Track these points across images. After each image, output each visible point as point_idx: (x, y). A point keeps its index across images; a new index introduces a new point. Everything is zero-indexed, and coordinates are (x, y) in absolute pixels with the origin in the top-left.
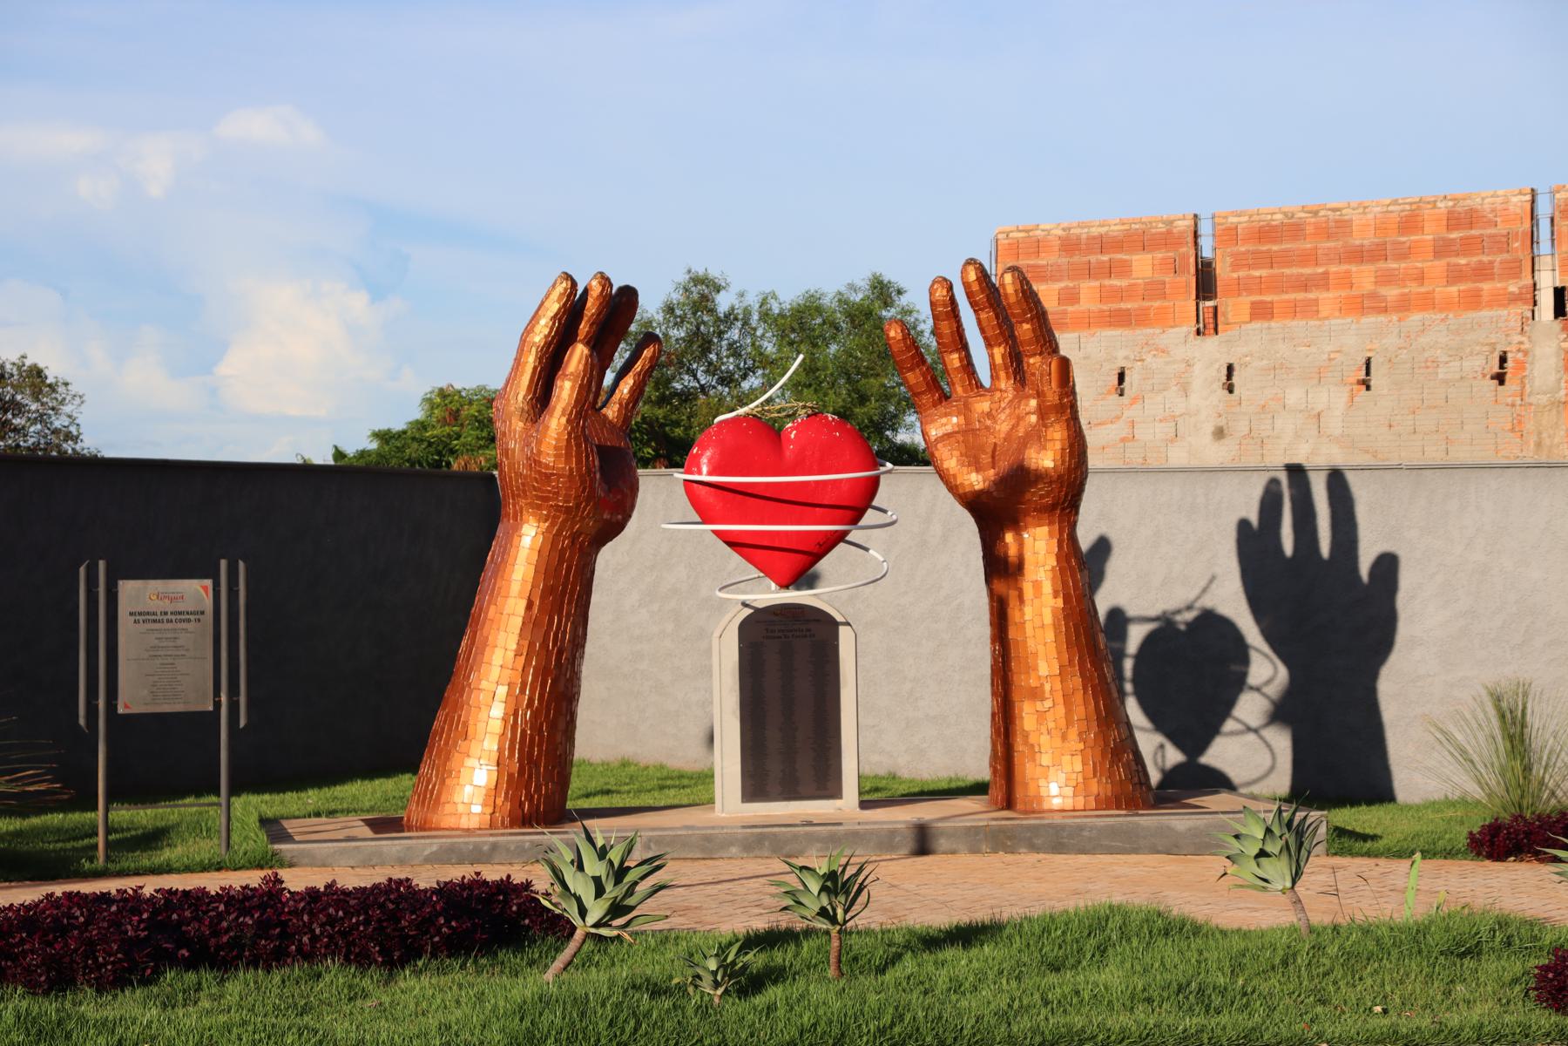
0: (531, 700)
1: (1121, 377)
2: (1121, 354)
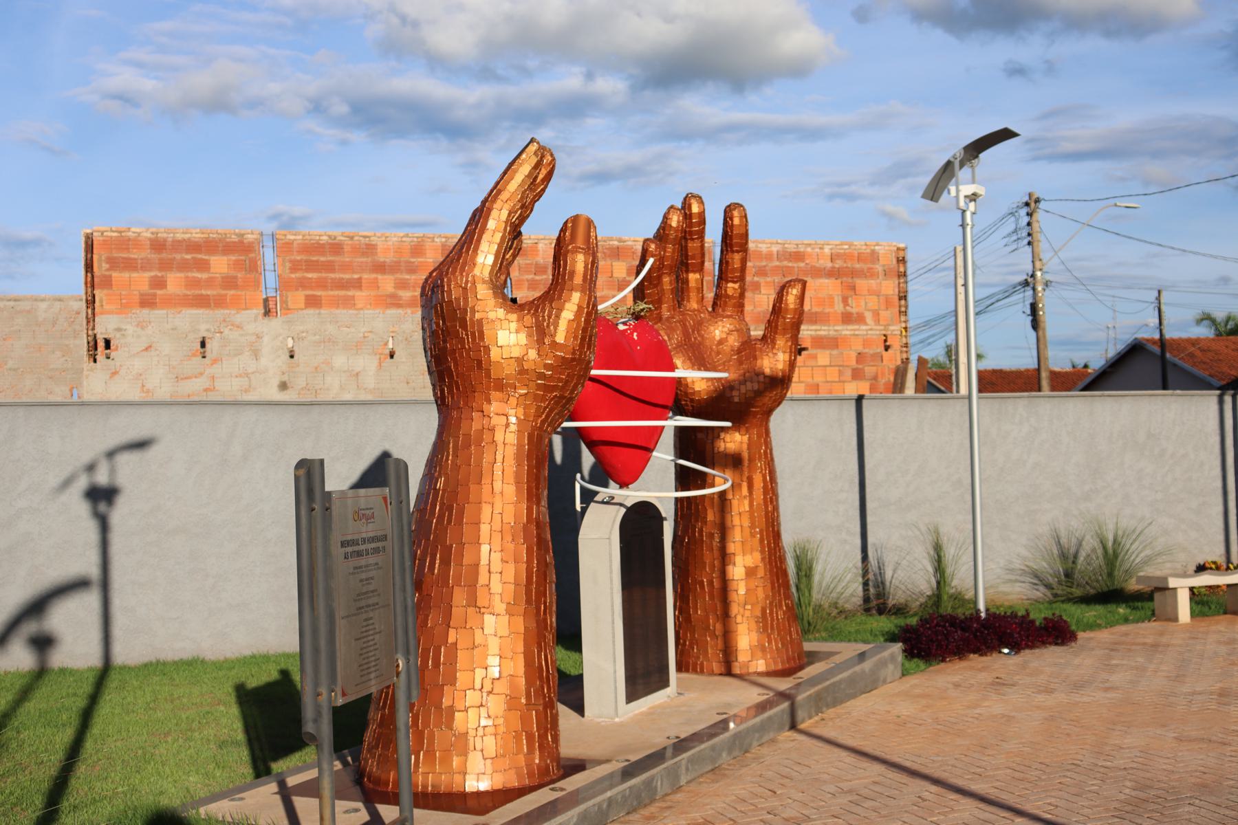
1: (203, 344)
2: (203, 327)
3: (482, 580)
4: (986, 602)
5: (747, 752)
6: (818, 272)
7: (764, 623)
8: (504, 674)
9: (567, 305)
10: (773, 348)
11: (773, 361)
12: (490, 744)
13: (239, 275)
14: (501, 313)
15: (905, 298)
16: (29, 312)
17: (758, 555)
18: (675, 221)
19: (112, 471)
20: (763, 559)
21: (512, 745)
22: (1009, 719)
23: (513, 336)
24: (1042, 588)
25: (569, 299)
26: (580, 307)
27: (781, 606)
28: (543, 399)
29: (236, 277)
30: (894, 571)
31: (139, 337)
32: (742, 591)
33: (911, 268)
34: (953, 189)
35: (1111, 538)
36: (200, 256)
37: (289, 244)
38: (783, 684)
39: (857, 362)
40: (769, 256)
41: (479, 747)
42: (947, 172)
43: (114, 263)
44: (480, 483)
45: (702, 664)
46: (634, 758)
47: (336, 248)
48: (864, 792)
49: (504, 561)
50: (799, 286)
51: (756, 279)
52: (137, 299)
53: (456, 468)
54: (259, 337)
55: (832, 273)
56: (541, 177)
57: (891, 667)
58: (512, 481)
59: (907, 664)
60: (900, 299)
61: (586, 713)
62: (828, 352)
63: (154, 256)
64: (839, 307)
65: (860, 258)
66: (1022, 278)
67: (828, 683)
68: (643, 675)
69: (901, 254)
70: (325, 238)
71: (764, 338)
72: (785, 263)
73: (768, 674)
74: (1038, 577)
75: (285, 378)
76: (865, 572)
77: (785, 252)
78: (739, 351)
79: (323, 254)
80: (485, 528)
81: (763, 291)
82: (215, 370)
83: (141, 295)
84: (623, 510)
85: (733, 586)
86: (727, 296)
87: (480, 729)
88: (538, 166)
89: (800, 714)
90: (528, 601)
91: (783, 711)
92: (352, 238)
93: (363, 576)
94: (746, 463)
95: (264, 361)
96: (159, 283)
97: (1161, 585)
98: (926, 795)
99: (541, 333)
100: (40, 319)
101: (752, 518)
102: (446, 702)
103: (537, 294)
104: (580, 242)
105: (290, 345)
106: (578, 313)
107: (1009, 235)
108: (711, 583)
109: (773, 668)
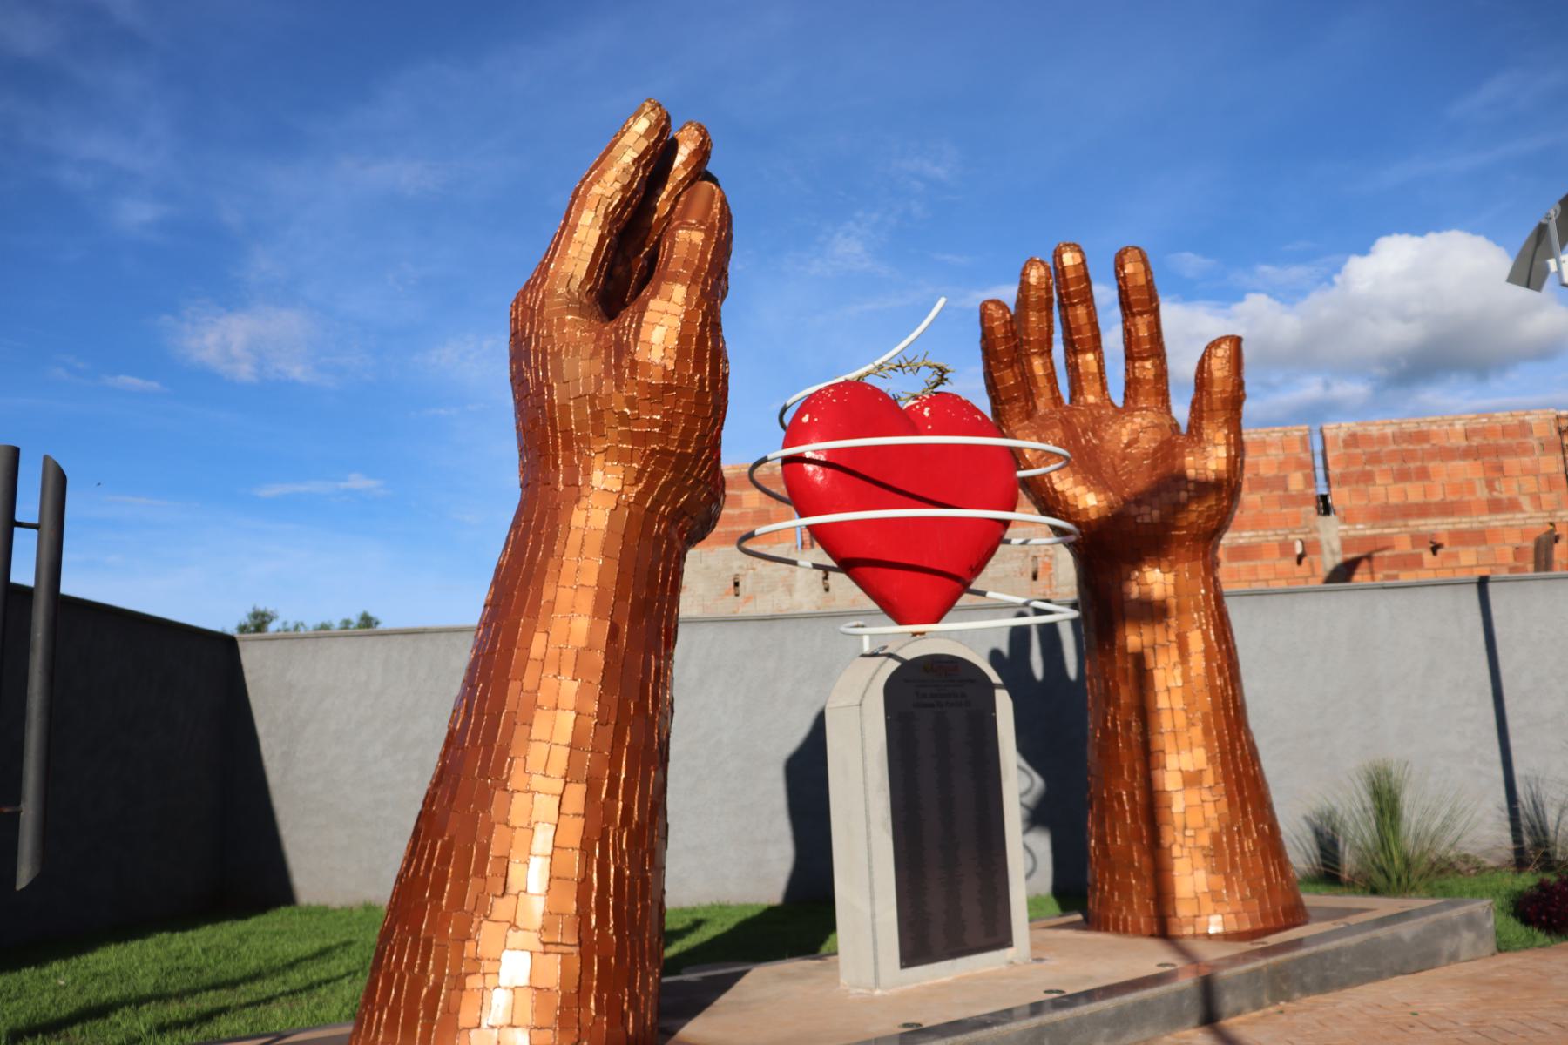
0: (627, 810)
1: (737, 584)
6: (1448, 454)
7: (1219, 855)
20: (1210, 760)
27: (1248, 832)
40: (1383, 440)
45: (1125, 920)
51: (1368, 468)
55: (1467, 453)
62: (1473, 549)
64: (1482, 493)
65: (1505, 431)
68: (921, 941)
72: (1405, 446)
81: (1378, 481)
94: (1174, 612)
108: (1131, 797)
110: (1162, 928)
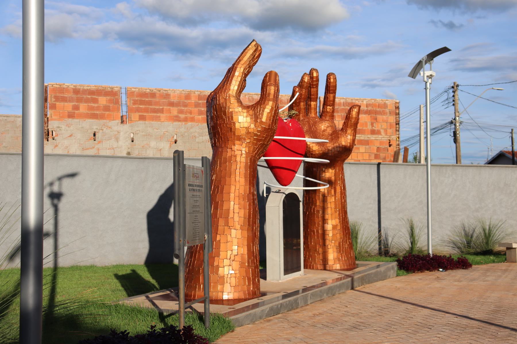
1: (95, 135)
3: (231, 215)
4: (432, 252)
5: (334, 295)
7: (340, 249)
8: (239, 253)
9: (267, 107)
10: (346, 133)
11: (345, 140)
12: (233, 281)
13: (111, 105)
14: (240, 109)
15: (399, 124)
16: (13, 122)
17: (338, 220)
18: (306, 79)
19: (60, 185)
20: (340, 222)
21: (242, 282)
22: (443, 288)
23: (245, 119)
24: (457, 249)
25: (268, 104)
26: (272, 108)
27: (347, 242)
28: (256, 144)
29: (109, 106)
30: (393, 239)
31: (67, 130)
32: (331, 235)
33: (402, 111)
34: (422, 73)
35: (487, 228)
36: (94, 97)
37: (133, 93)
38: (348, 273)
39: (377, 151)
41: (229, 282)
42: (419, 65)
43: (57, 99)
44: (230, 177)
46: (289, 292)
47: (153, 95)
48: (384, 307)
49: (240, 208)
50: (358, 108)
52: (67, 114)
53: (221, 171)
54: (119, 132)
56: (256, 56)
57: (392, 271)
58: (243, 177)
59: (399, 271)
60: (396, 124)
61: (267, 279)
62: (364, 146)
63: (75, 96)
64: (369, 127)
65: (379, 106)
66: (450, 119)
67: (366, 273)
68: (291, 267)
69: (397, 105)
70: (148, 90)
71: (342, 129)
73: (341, 270)
74: (455, 244)
75: (129, 150)
76: (380, 238)
77: (346, 102)
78: (331, 135)
79: (147, 97)
80: (232, 195)
82: (99, 146)
83: (69, 112)
84: (284, 196)
85: (327, 232)
86: (327, 112)
87: (229, 275)
88: (255, 51)
89: (355, 284)
90: (249, 225)
91: (348, 281)
92: (160, 91)
93: (195, 199)
95: (120, 143)
96: (76, 108)
97: (509, 247)
98: (408, 308)
99: (256, 118)
100: (18, 125)
101: (335, 205)
102: (216, 264)
103: (251, 104)
104: (272, 82)
105: (132, 136)
106: (271, 110)
107: (444, 101)
109: (343, 268)
110: (325, 267)
